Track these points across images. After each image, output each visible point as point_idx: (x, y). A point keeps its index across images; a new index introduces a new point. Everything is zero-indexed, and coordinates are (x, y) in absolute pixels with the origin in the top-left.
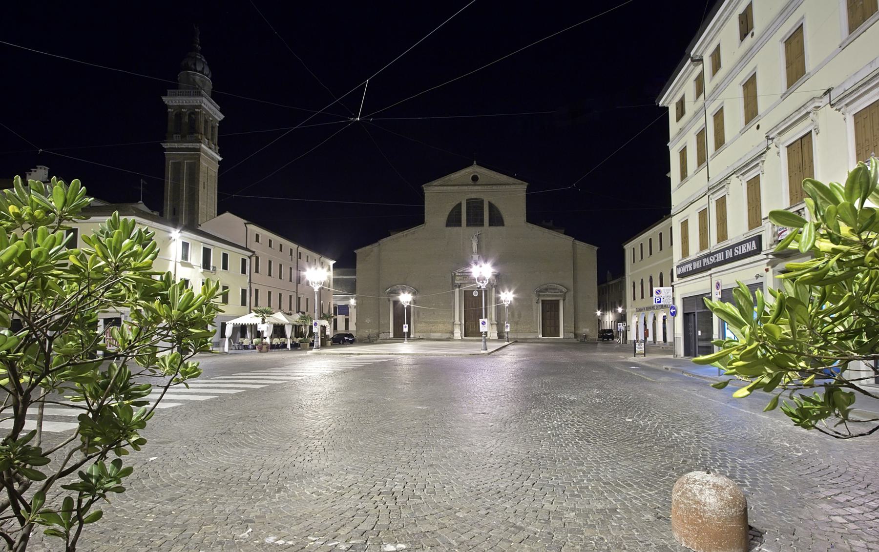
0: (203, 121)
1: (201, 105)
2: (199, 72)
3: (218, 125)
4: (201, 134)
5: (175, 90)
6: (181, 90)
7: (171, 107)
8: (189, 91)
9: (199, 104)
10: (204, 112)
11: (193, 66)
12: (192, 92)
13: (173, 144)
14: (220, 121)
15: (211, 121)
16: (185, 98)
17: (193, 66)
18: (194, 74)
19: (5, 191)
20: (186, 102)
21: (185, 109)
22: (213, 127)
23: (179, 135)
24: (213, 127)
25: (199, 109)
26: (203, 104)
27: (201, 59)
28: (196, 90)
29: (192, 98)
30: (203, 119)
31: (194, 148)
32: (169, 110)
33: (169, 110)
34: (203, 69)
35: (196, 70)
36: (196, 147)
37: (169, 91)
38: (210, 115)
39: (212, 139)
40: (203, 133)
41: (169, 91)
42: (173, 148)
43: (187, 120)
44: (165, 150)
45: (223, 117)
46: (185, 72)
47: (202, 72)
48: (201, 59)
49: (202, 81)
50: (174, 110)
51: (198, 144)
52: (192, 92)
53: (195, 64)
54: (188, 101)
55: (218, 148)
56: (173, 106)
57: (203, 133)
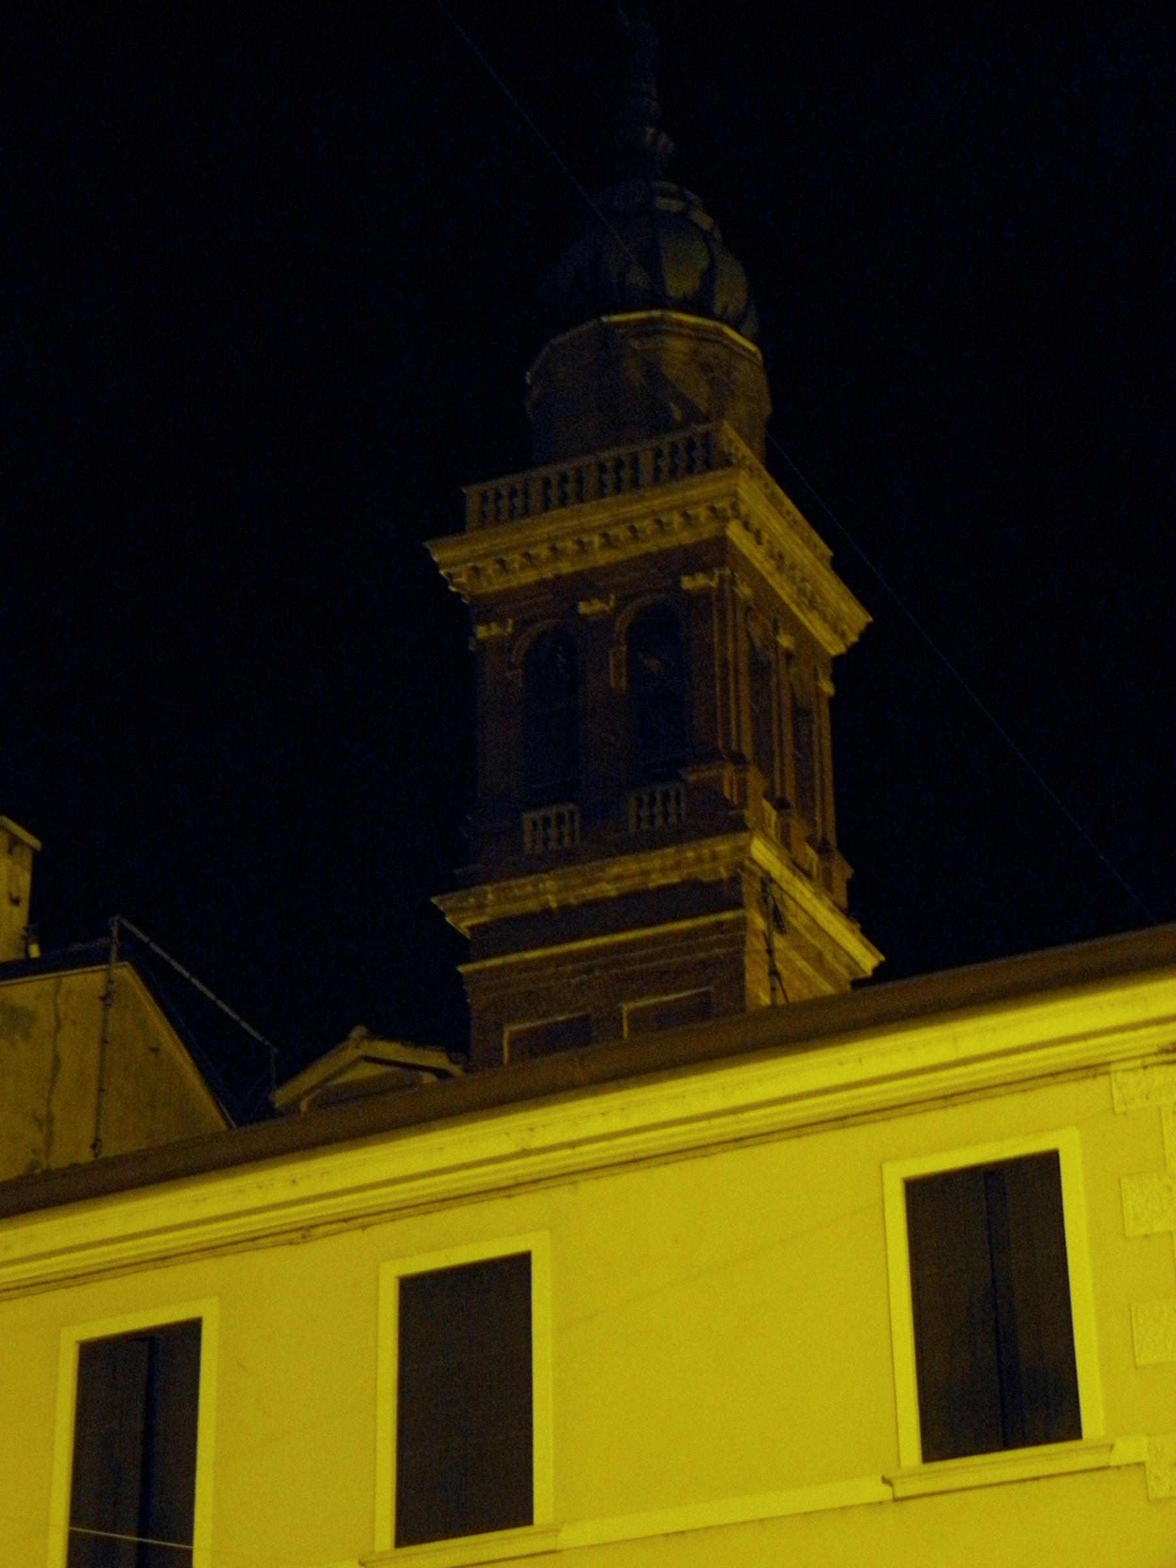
0: (743, 666)
1: (721, 544)
2: (685, 305)
3: (828, 688)
4: (738, 759)
5: (517, 479)
6: (565, 467)
7: (488, 608)
8: (623, 451)
9: (708, 531)
10: (745, 591)
11: (637, 278)
12: (646, 461)
13: (523, 886)
14: (838, 660)
15: (789, 656)
16: (596, 515)
17: (637, 278)
18: (645, 330)
19: (528, 381)
20: (609, 542)
21: (603, 595)
22: (801, 714)
23: (566, 809)
24: (801, 714)
25: (706, 569)
26: (734, 531)
27: (683, 216)
28: (678, 437)
29: (658, 500)
30: (744, 646)
31: (692, 886)
32: (481, 632)
33: (481, 632)
34: (708, 277)
35: (656, 299)
36: (705, 873)
37: (473, 493)
38: (781, 617)
39: (807, 811)
40: (747, 750)
41: (473, 493)
42: (528, 918)
43: (617, 680)
44: (461, 948)
45: (856, 618)
46: (586, 327)
47: (700, 304)
48: (683, 216)
49: (705, 368)
50: (520, 626)
51: (723, 847)
52: (646, 461)
53: (651, 261)
54: (621, 532)
55: (842, 872)
56: (507, 596)
57: (747, 750)
